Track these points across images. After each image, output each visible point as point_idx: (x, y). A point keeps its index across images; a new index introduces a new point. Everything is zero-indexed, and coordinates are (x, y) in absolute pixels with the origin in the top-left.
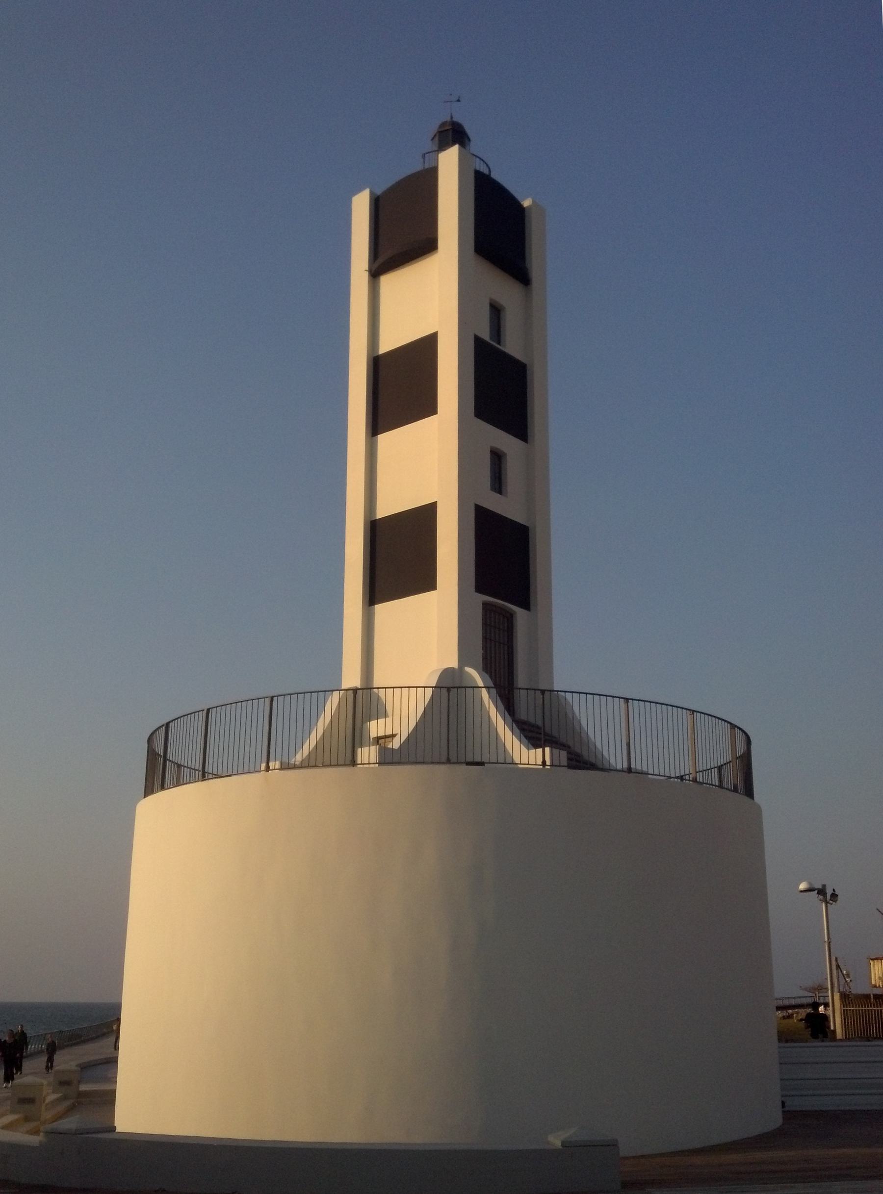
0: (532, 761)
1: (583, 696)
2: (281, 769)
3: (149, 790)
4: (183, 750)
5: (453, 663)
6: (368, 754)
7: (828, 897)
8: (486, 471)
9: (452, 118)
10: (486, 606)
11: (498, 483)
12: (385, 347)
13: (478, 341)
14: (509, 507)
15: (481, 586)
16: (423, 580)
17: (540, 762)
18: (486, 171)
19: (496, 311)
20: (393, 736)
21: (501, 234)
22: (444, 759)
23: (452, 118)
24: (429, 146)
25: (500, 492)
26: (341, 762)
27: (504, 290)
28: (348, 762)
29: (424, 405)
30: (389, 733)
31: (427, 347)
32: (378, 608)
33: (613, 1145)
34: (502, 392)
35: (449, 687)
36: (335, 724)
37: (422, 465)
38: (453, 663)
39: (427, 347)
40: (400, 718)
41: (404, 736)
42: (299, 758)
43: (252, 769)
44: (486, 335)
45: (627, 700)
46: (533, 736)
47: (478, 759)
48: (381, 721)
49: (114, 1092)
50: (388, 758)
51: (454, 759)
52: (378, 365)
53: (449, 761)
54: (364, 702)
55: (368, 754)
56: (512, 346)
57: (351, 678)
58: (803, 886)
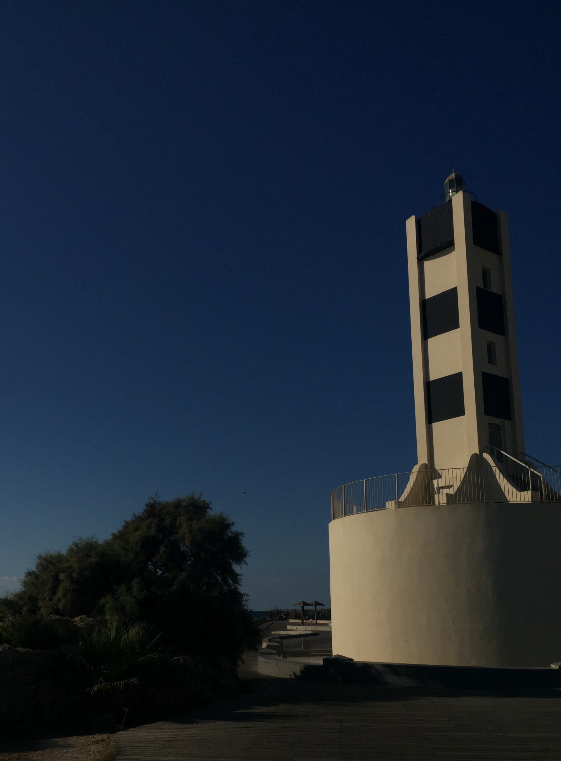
0: (526, 499)
5: (477, 451)
8: (483, 353)
11: (491, 360)
12: (428, 295)
13: (478, 288)
14: (498, 370)
15: (486, 413)
19: (485, 273)
20: (451, 486)
21: (484, 232)
25: (492, 363)
27: (489, 259)
31: (452, 294)
33: (353, 660)
35: (476, 462)
37: (452, 353)
38: (477, 451)
39: (452, 294)
44: (481, 286)
46: (521, 486)
47: (448, 484)
48: (440, 480)
49: (330, 633)
52: (424, 304)
56: (495, 289)
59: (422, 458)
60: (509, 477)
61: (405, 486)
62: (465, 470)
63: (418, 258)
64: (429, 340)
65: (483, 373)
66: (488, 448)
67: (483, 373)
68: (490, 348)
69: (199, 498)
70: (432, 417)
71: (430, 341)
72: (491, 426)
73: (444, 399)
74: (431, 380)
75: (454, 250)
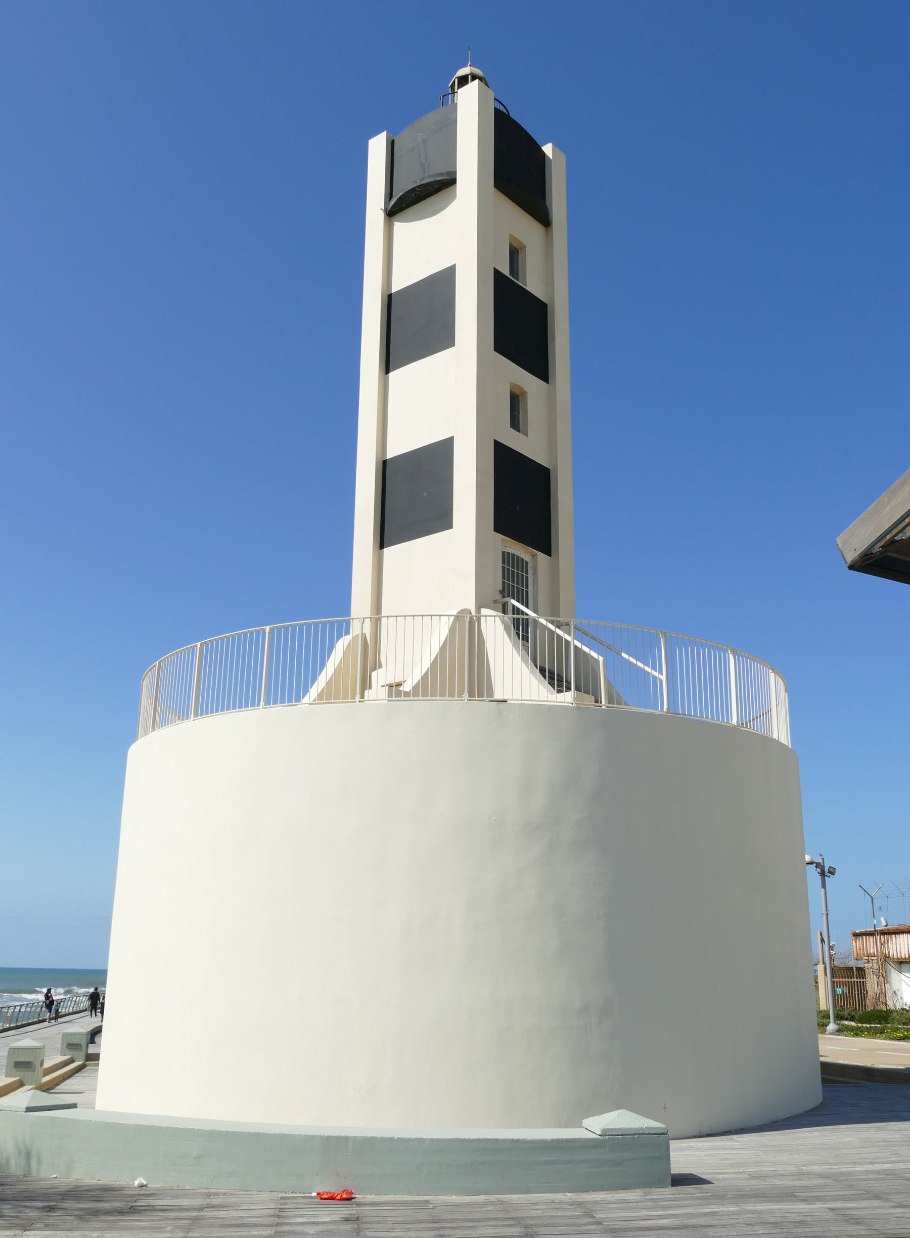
5: (471, 606)
7: (826, 870)
11: (516, 422)
13: (497, 274)
19: (515, 253)
21: (517, 170)
27: (524, 227)
30: (398, 680)
31: (444, 281)
34: (520, 327)
35: (467, 630)
44: (506, 271)
56: (533, 284)
58: (808, 858)
59: (359, 626)
60: (542, 671)
61: (323, 665)
62: (452, 618)
64: (385, 549)
65: (498, 446)
66: (495, 602)
67: (498, 446)
68: (516, 400)
70: (384, 538)
71: (386, 550)
72: (507, 557)
73: (412, 497)
74: (393, 291)
75: (455, 198)
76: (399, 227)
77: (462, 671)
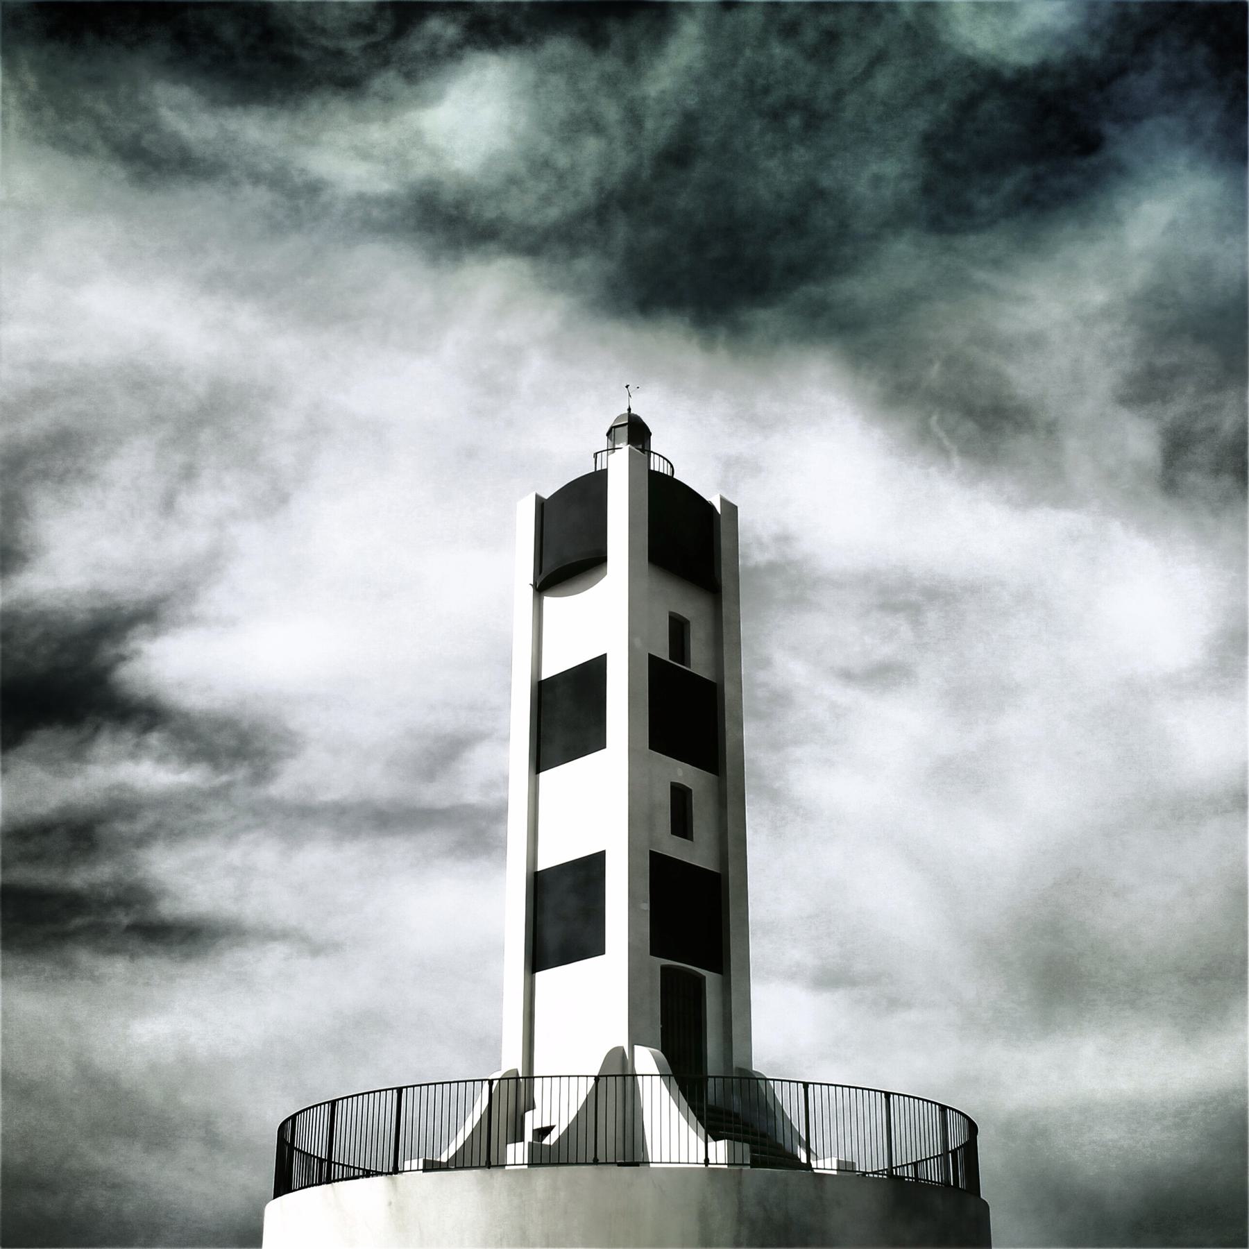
0: (693, 1160)
1: (866, 1092)
2: (425, 1170)
3: (277, 1195)
4: (312, 1140)
5: (624, 1043)
6: (517, 1153)
9: (629, 410)
10: (664, 969)
11: (682, 825)
13: (653, 660)
15: (656, 950)
16: (586, 943)
17: (702, 1160)
18: (667, 471)
19: (678, 629)
22: (590, 1159)
23: (629, 410)
24: (603, 443)
26: (476, 1164)
27: (691, 607)
28: (483, 1164)
29: (588, 737)
30: (546, 1124)
32: (538, 974)
35: (616, 1077)
36: (582, 1118)
40: (555, 1108)
41: (564, 1127)
42: (444, 1159)
43: (476, 1164)
44: (665, 655)
45: (888, 1095)
50: (540, 1157)
51: (601, 1160)
53: (596, 1162)
54: (517, 1092)
55: (517, 1153)
56: (699, 663)
57: (512, 1061)
63: (534, 585)
68: (680, 796)
69: (707, 1162)
76: (549, 601)
77: (606, 1134)
